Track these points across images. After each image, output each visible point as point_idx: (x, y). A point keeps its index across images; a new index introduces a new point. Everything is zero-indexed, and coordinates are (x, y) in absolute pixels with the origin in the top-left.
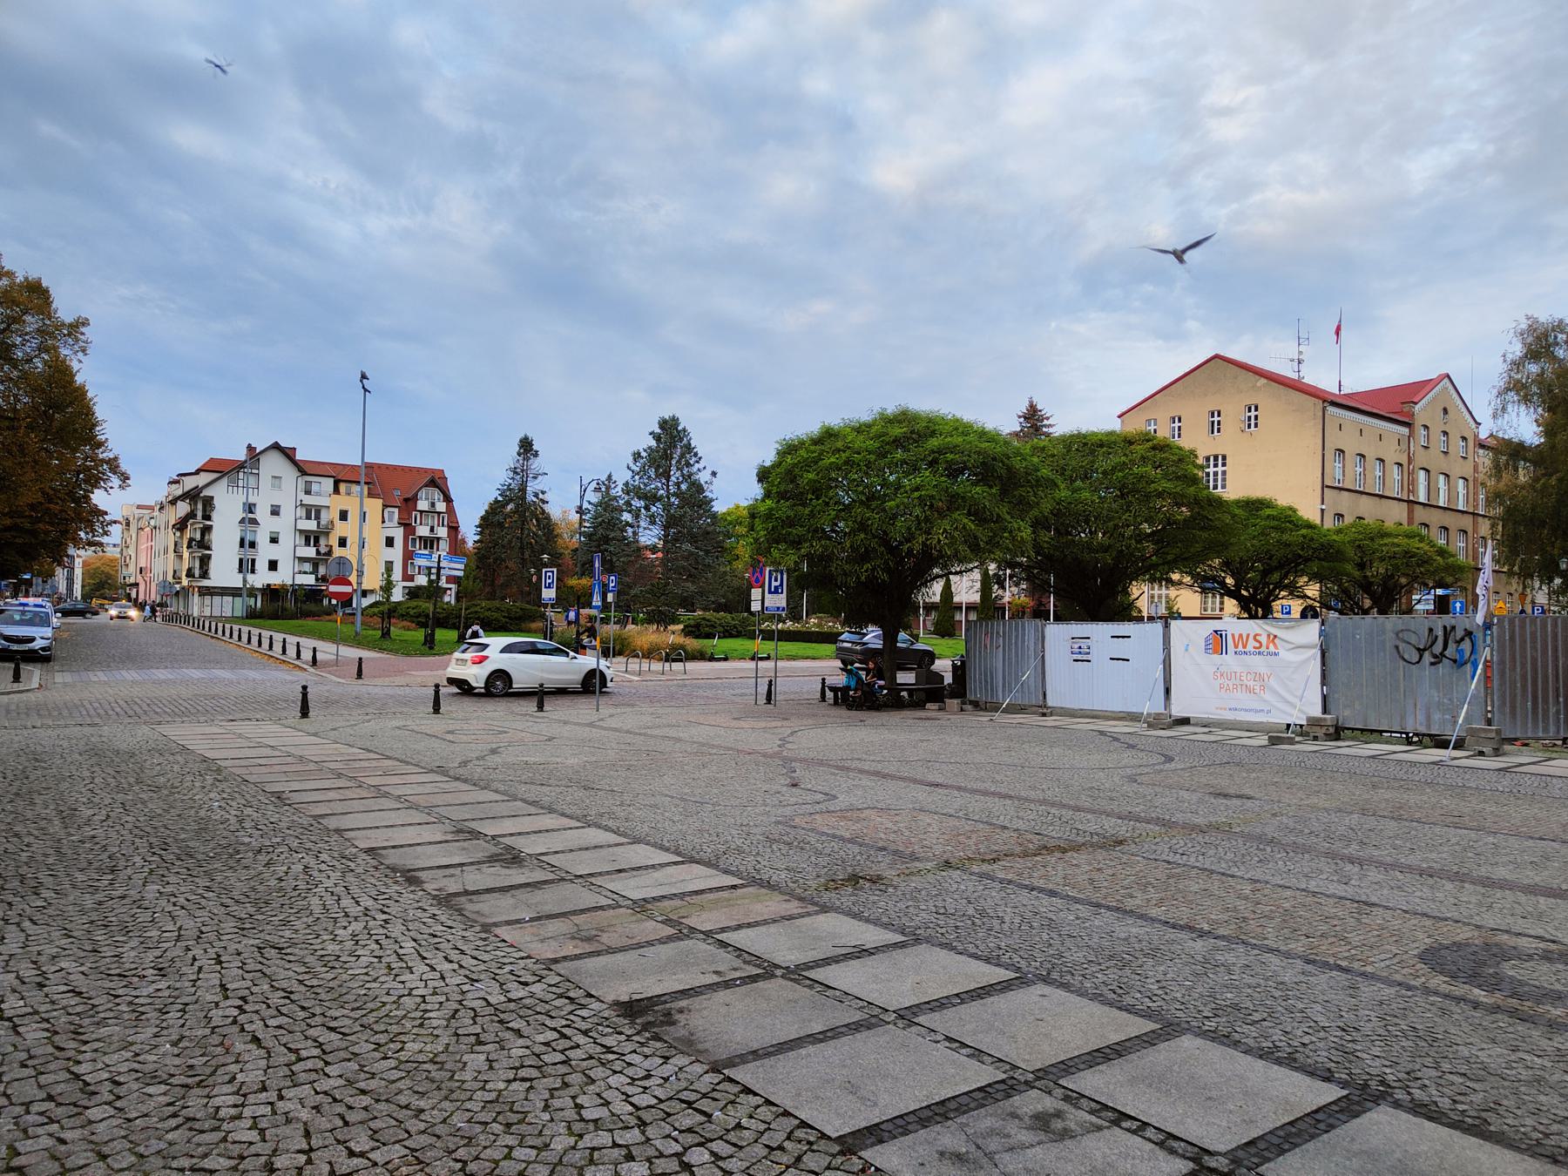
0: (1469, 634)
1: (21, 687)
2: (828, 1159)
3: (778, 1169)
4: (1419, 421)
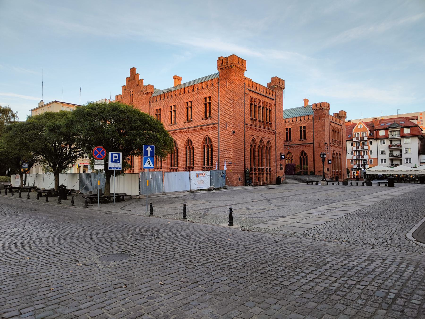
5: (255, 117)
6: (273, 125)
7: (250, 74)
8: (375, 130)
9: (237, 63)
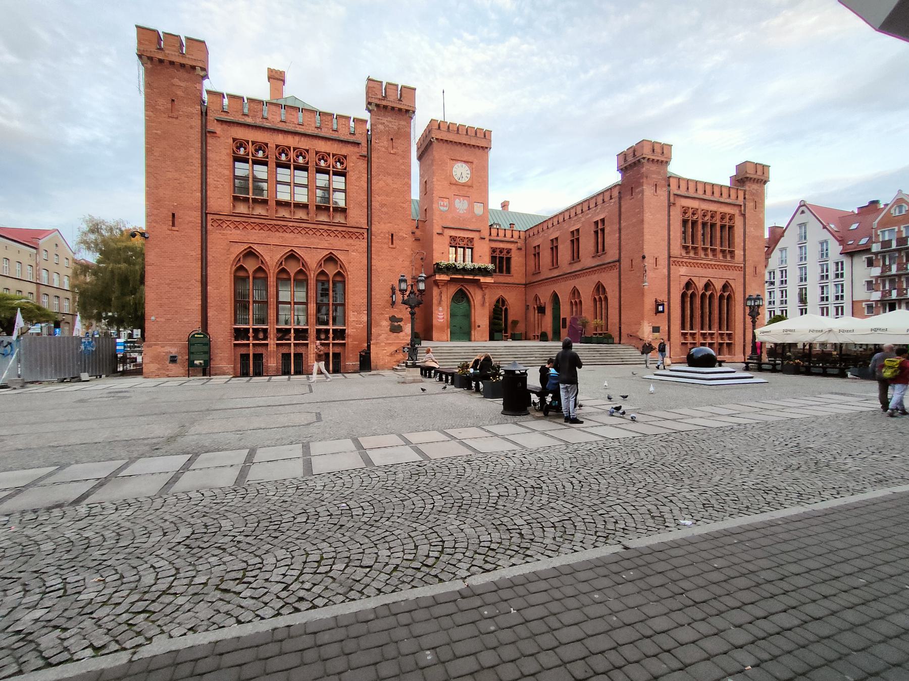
0: (10, 344)
1: (174, 228)
2: (659, 650)
3: (718, 673)
4: (41, 249)
5: (693, 243)
6: (739, 253)
7: (680, 166)
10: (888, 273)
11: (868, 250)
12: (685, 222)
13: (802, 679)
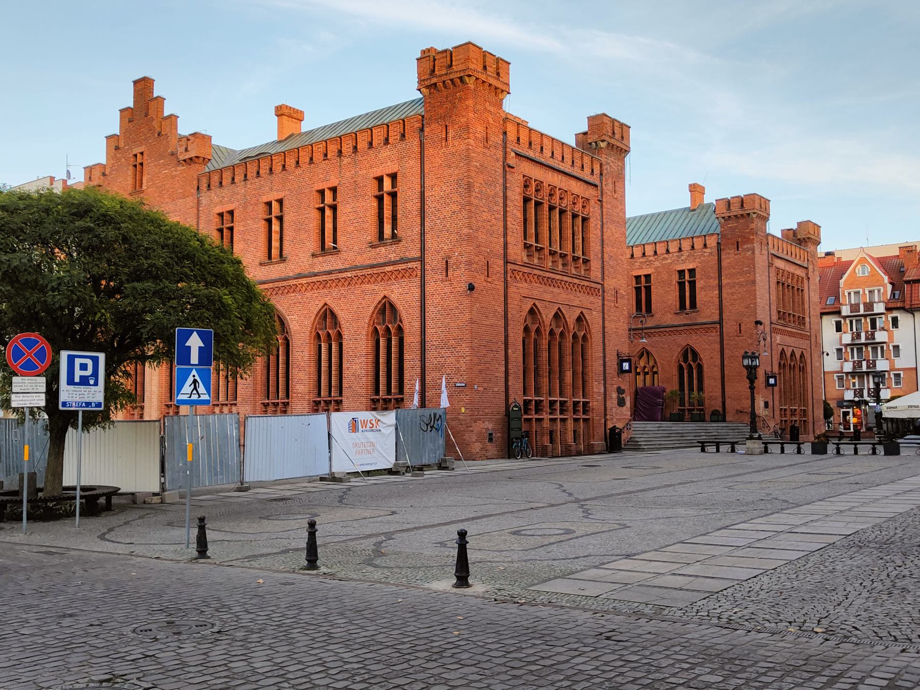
8: (908, 282)
9: (480, 69)
10: (857, 342)
11: (838, 313)
12: (526, 200)
13: (861, 686)
